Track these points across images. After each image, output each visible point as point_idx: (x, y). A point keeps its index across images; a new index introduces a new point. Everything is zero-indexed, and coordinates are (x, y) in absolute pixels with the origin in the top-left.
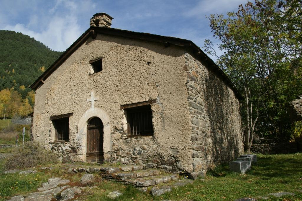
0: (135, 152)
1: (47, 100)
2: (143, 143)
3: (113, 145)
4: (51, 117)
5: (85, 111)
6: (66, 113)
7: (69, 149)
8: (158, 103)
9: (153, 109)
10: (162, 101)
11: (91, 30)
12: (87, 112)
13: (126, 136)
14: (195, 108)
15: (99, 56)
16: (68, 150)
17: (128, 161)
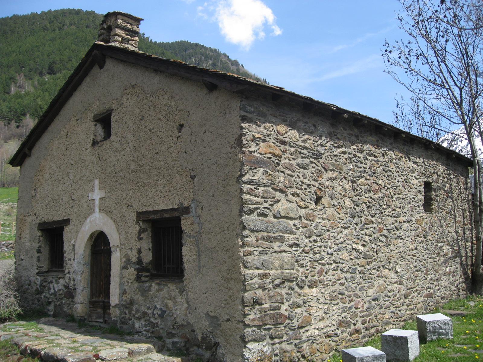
0: (155, 312)
1: (35, 190)
2: (167, 296)
3: (124, 292)
4: (39, 223)
5: (86, 218)
6: (61, 219)
7: (64, 289)
8: (192, 214)
9: (184, 228)
10: (199, 211)
11: (93, 51)
12: (88, 220)
13: (148, 274)
14: (265, 231)
15: (107, 106)
16: (61, 292)
17: (144, 329)
